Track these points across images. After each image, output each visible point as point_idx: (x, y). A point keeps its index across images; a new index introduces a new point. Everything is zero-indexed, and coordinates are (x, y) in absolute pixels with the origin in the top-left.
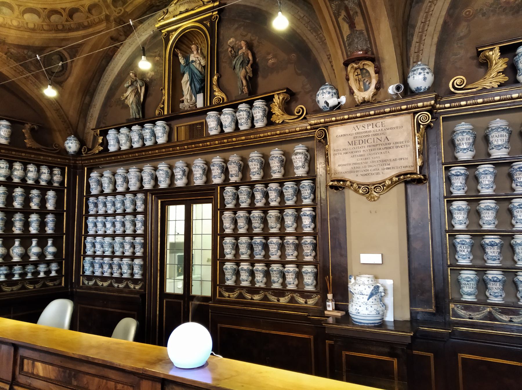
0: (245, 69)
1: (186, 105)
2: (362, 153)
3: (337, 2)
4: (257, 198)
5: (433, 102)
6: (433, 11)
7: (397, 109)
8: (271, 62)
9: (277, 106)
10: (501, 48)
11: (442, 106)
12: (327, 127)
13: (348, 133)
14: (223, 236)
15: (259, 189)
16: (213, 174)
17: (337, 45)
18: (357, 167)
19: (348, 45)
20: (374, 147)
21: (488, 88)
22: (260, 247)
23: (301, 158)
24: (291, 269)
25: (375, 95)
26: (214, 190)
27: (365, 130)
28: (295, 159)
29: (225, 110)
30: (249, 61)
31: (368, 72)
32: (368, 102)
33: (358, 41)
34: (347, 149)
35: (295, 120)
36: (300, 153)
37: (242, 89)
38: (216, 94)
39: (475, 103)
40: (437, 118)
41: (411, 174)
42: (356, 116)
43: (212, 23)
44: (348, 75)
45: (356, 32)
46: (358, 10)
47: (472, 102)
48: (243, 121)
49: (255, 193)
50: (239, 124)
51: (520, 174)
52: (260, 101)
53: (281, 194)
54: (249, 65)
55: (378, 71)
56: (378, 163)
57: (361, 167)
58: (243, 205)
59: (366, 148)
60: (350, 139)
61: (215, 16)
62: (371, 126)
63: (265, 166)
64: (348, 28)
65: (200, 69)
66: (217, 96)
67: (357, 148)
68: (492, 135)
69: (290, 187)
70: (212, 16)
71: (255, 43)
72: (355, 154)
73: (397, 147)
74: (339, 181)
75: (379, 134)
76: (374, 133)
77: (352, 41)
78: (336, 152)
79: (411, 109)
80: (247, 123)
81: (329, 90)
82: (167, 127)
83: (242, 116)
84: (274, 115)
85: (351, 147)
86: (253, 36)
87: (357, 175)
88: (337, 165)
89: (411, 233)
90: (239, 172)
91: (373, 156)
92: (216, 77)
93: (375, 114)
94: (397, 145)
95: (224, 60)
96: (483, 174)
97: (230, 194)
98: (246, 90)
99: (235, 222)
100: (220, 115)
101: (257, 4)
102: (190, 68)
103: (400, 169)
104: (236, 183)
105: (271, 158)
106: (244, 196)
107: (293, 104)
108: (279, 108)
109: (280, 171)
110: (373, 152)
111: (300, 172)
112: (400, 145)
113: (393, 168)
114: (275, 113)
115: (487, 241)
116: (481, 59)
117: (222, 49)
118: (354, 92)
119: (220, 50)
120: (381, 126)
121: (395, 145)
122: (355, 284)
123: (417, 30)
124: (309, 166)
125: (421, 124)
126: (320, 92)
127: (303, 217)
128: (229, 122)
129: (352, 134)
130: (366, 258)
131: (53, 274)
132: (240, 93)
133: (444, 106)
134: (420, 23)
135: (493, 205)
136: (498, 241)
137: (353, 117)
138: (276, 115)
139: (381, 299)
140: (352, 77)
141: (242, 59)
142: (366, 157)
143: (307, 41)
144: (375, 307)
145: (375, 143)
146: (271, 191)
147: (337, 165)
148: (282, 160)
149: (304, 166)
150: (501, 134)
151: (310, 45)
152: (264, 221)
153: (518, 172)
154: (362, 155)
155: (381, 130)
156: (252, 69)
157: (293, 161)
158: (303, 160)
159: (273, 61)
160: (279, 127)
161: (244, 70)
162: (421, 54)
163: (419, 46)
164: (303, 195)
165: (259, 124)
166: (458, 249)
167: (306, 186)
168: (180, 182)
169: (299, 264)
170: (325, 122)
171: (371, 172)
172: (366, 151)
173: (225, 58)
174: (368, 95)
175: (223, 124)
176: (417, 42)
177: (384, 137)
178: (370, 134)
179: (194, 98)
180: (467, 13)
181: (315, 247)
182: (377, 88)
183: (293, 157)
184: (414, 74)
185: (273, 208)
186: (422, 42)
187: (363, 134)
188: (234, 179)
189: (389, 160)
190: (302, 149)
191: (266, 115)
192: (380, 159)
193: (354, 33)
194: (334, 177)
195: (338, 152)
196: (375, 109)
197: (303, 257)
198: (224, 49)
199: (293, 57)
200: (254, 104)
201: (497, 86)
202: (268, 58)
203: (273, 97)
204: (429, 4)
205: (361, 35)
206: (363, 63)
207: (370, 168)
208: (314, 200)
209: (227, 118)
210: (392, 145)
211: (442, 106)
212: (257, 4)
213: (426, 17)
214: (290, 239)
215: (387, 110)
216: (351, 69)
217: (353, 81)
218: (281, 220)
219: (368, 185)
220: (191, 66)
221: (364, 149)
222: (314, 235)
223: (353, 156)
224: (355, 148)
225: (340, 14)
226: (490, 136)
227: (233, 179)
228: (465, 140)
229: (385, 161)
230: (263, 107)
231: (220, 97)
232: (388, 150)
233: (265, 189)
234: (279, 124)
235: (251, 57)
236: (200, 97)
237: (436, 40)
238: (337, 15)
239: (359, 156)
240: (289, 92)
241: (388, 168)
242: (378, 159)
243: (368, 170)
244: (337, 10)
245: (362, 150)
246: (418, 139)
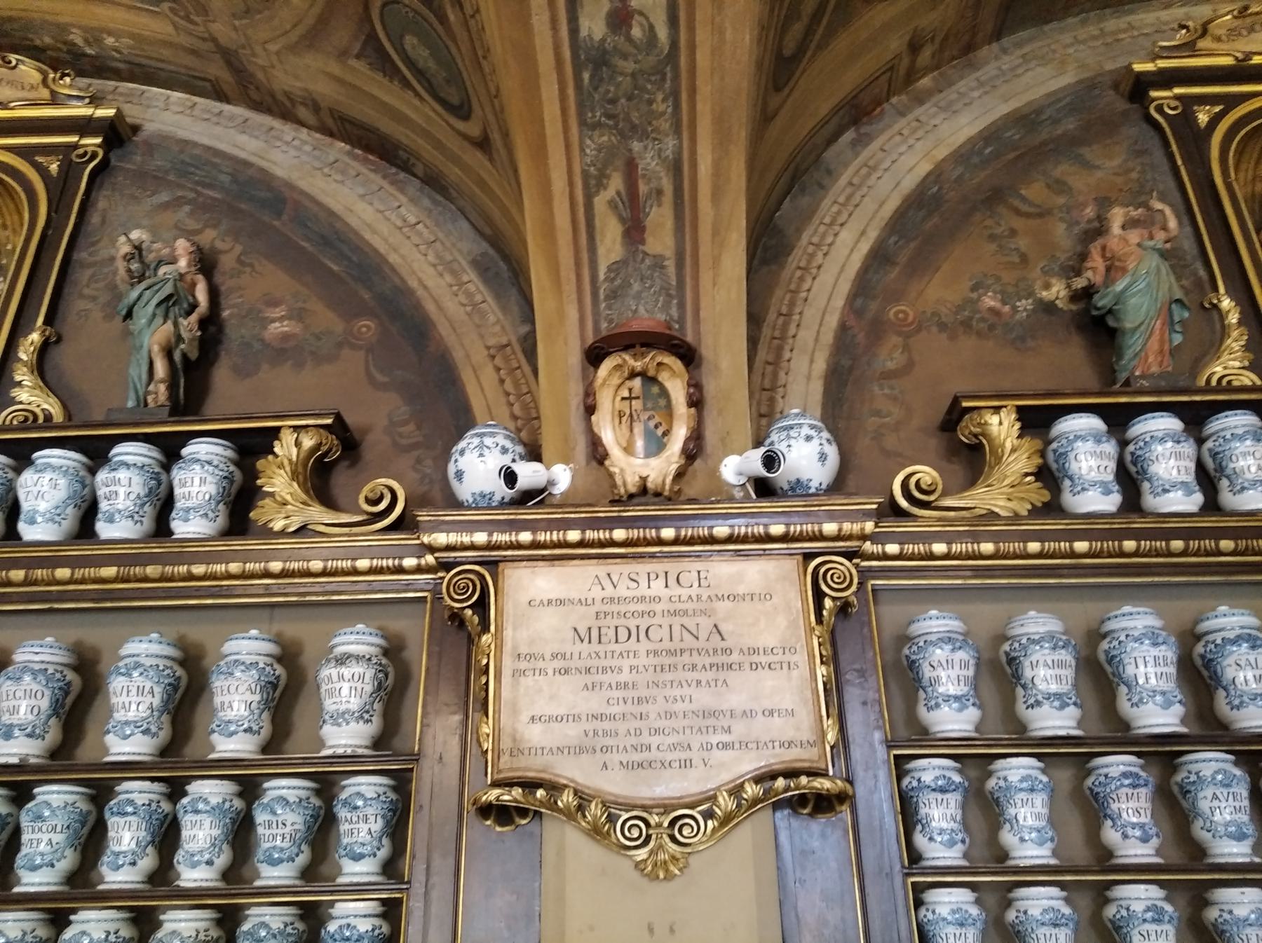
0: (176, 324)
2: (625, 677)
3: (605, 138)
4: (117, 849)
6: (809, 290)
7: (753, 533)
8: (276, 328)
9: (288, 469)
12: (492, 565)
13: (575, 595)
15: (140, 803)
17: (570, 287)
18: (605, 733)
19: (607, 298)
21: (1003, 513)
23: (362, 678)
25: (679, 475)
27: (638, 593)
28: (335, 678)
31: (664, 393)
33: (641, 292)
34: (568, 656)
35: (355, 530)
36: (358, 658)
37: (141, 393)
39: (973, 551)
41: (791, 774)
42: (611, 539)
44: (595, 394)
45: (643, 260)
46: (667, 185)
47: (964, 550)
50: (100, 516)
51: (1130, 795)
52: (217, 444)
54: (194, 317)
56: (686, 722)
57: (622, 731)
59: (643, 660)
61: (90, 149)
62: (661, 581)
64: (619, 239)
66: (21, 403)
67: (609, 655)
68: (1034, 658)
69: (291, 800)
70: (75, 146)
71: (227, 262)
72: (600, 677)
73: (754, 666)
74: (530, 785)
75: (690, 612)
76: (672, 607)
77: (621, 287)
78: (523, 665)
80: (136, 517)
84: (267, 501)
85: (579, 647)
86: (223, 241)
87: (605, 766)
88: (525, 717)
90: (50, 717)
91: (670, 692)
92: (35, 337)
93: (676, 541)
94: (755, 659)
95: (86, 291)
96: (1021, 790)
98: (161, 391)
100: (18, 471)
101: (255, 154)
103: (770, 752)
105: (224, 669)
106: (52, 835)
108: (294, 476)
109: (255, 728)
110: (668, 676)
112: (763, 659)
113: (744, 745)
114: (272, 495)
116: (967, 433)
117: (90, 255)
118: (607, 455)
119: (81, 255)
120: (696, 584)
121: (747, 660)
125: (827, 595)
128: (53, 503)
129: (590, 601)
132: (130, 404)
133: (883, 549)
134: (775, 315)
137: (599, 539)
138: (276, 501)
140: (606, 402)
141: (168, 289)
142: (644, 692)
143: (420, 293)
145: (676, 645)
146: (199, 817)
147: (525, 717)
148: (272, 679)
149: (367, 712)
150: (1060, 657)
151: (430, 307)
153: (1124, 790)
154: (626, 685)
155: (695, 598)
156: (199, 333)
157: (324, 687)
158: (369, 688)
159: (286, 329)
161: (169, 326)
162: (783, 397)
164: (345, 841)
165: (186, 527)
167: (366, 800)
170: (489, 547)
171: (660, 755)
172: (641, 669)
173: (94, 285)
175: (25, 506)
176: (769, 363)
177: (706, 624)
178: (658, 608)
180: (901, 316)
184: (789, 437)
186: (784, 364)
187: (633, 607)
188: (15, 751)
189: (728, 714)
190: (368, 644)
191: (227, 499)
192: (694, 707)
193: (635, 261)
194: (509, 766)
195: (531, 666)
196: (679, 524)
198: (98, 258)
199: (364, 329)
200: (185, 452)
201: (1026, 513)
202: (267, 315)
203: (275, 433)
204: (799, 273)
205: (656, 274)
206: (659, 359)
207: (655, 740)
210: (735, 657)
212: (255, 154)
216: (610, 374)
217: (609, 417)
219: (644, 808)
221: (634, 662)
223: (590, 686)
224: (602, 654)
225: (605, 181)
226: (1027, 663)
228: (957, 667)
229: (713, 714)
230: (221, 466)
231: (37, 411)
232: (722, 675)
233: (166, 806)
234: (283, 533)
235: (201, 295)
237: (820, 365)
238: (594, 183)
239: (614, 686)
240: (339, 428)
241: (725, 746)
242: (685, 706)
243: (649, 748)
244: (599, 165)
245: (626, 663)
246: (820, 645)
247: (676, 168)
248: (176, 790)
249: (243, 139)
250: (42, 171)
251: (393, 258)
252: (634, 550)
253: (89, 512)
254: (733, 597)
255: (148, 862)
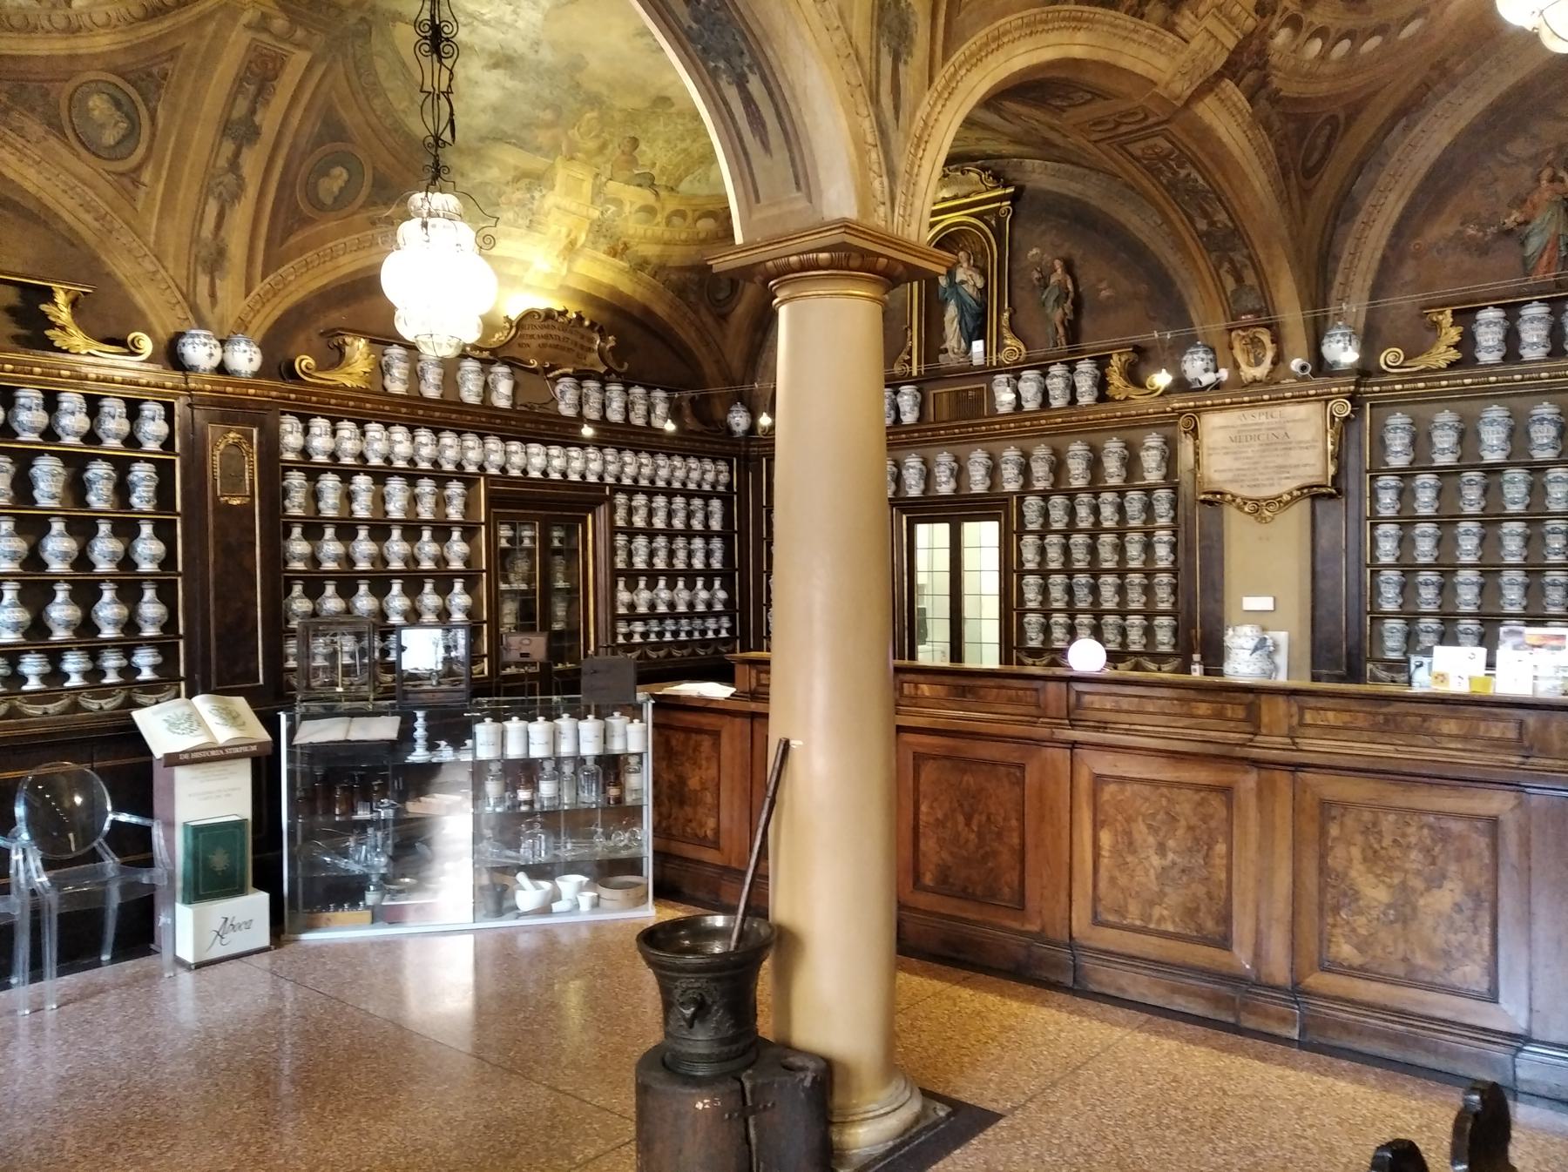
1: (950, 360)
2: (1250, 454)
5: (1352, 388)
8: (1104, 294)
10: (1454, 313)
11: (1368, 389)
14: (1022, 574)
16: (1006, 477)
20: (1268, 446)
22: (1086, 591)
24: (1137, 622)
26: (1006, 500)
29: (1026, 374)
30: (1067, 294)
32: (1261, 381)
36: (1153, 448)
38: (1008, 342)
40: (1362, 407)
41: (1312, 487)
43: (1000, 221)
46: (1248, 262)
48: (1058, 392)
49: (1078, 507)
53: (1121, 509)
55: (1276, 340)
58: (1057, 526)
60: (1232, 432)
63: (1095, 464)
65: (974, 294)
71: (1078, 262)
74: (1215, 493)
79: (1323, 394)
81: (1202, 355)
82: (918, 394)
83: (1057, 385)
89: (1319, 568)
93: (1270, 400)
97: (1035, 508)
99: (1042, 551)
102: (958, 293)
104: (1045, 491)
107: (1142, 366)
111: (1153, 476)
113: (1294, 478)
115: (1421, 579)
119: (1015, 266)
122: (1233, 637)
123: (1342, 265)
124: (1167, 467)
126: (1187, 357)
127: (1157, 545)
130: (1252, 603)
131: (724, 634)
135: (1431, 531)
136: (1434, 579)
139: (1270, 655)
140: (1237, 345)
144: (1259, 664)
152: (1093, 550)
160: (1119, 406)
161: (1060, 310)
163: (1344, 291)
166: (1382, 590)
168: (945, 488)
169: (1149, 614)
170: (1195, 407)
174: (1260, 372)
177: (1282, 432)
179: (963, 344)
181: (1175, 590)
182: (1275, 363)
183: (1143, 453)
185: (1108, 531)
194: (1207, 487)
197: (1155, 604)
203: (1110, 356)
208: (1174, 519)
209: (1029, 386)
211: (1368, 389)
213: (1357, 246)
214: (1136, 578)
215: (1288, 394)
218: (1121, 549)
220: (960, 291)
222: (1174, 571)
227: (1040, 485)
234: (1119, 400)
235: (1070, 287)
236: (978, 346)
237: (1369, 282)
247: (1250, 257)
248: (1096, 496)
249: (1073, 185)
250: (987, 223)
251: (1152, 247)
252: (1253, 404)
253: (1045, 394)
254: (1294, 421)
255: (1092, 519)
